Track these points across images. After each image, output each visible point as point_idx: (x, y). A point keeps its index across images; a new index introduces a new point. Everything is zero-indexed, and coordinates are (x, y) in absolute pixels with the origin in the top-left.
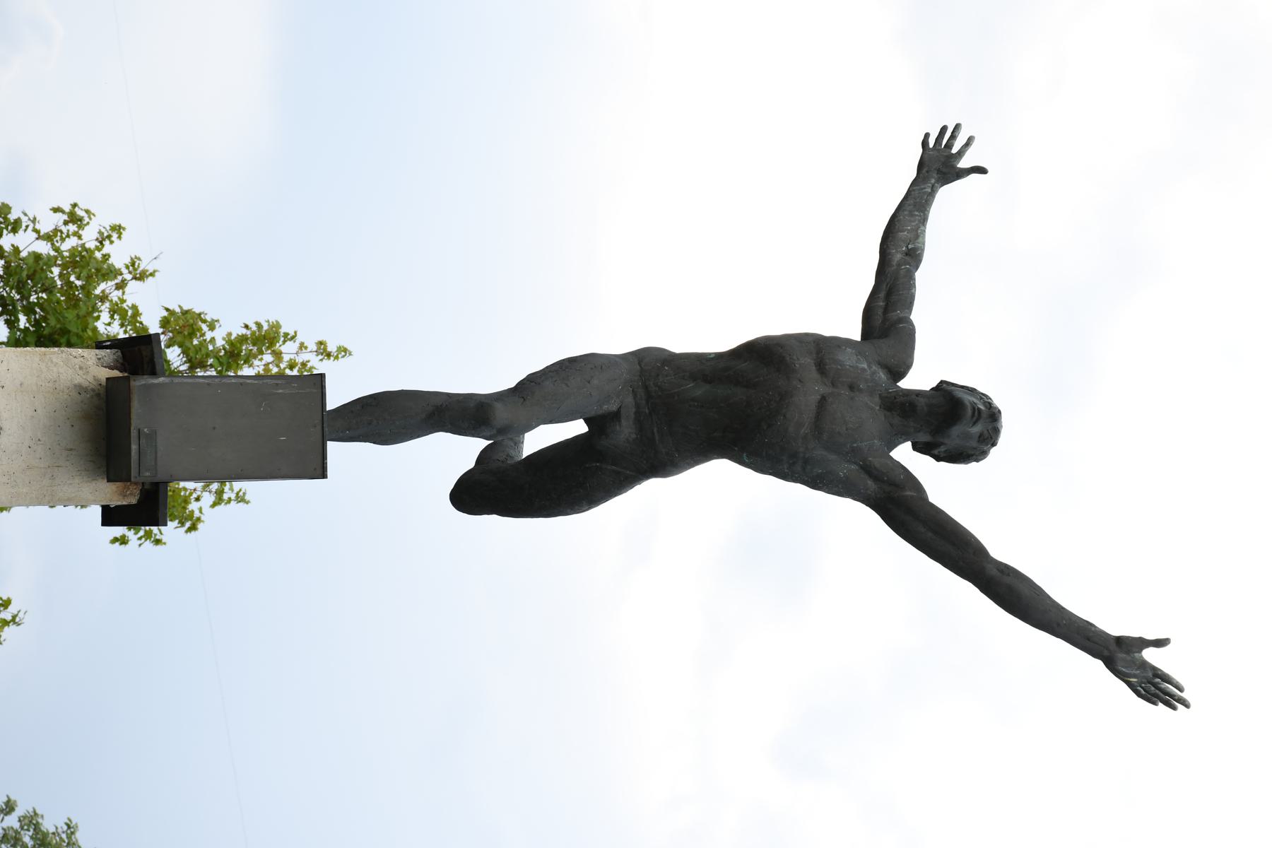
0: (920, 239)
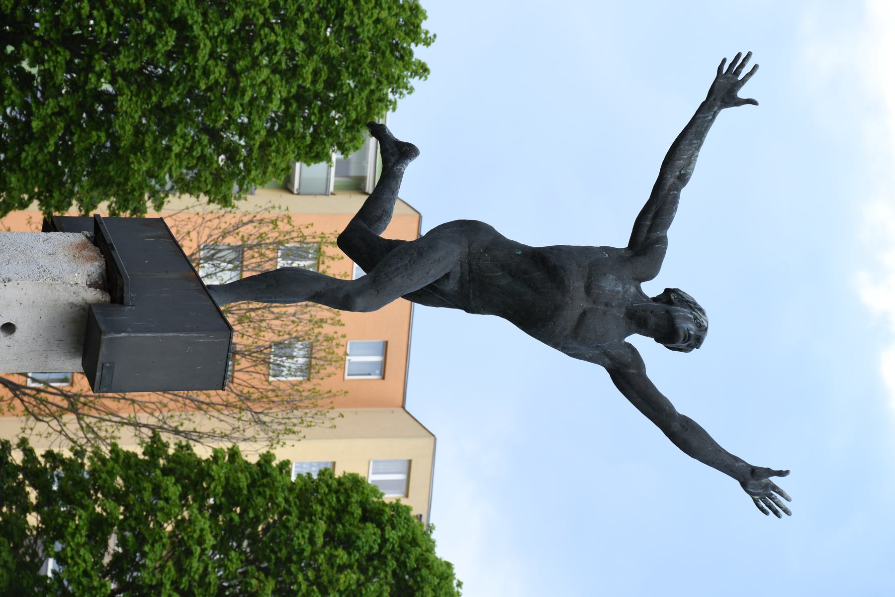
0: (692, 165)
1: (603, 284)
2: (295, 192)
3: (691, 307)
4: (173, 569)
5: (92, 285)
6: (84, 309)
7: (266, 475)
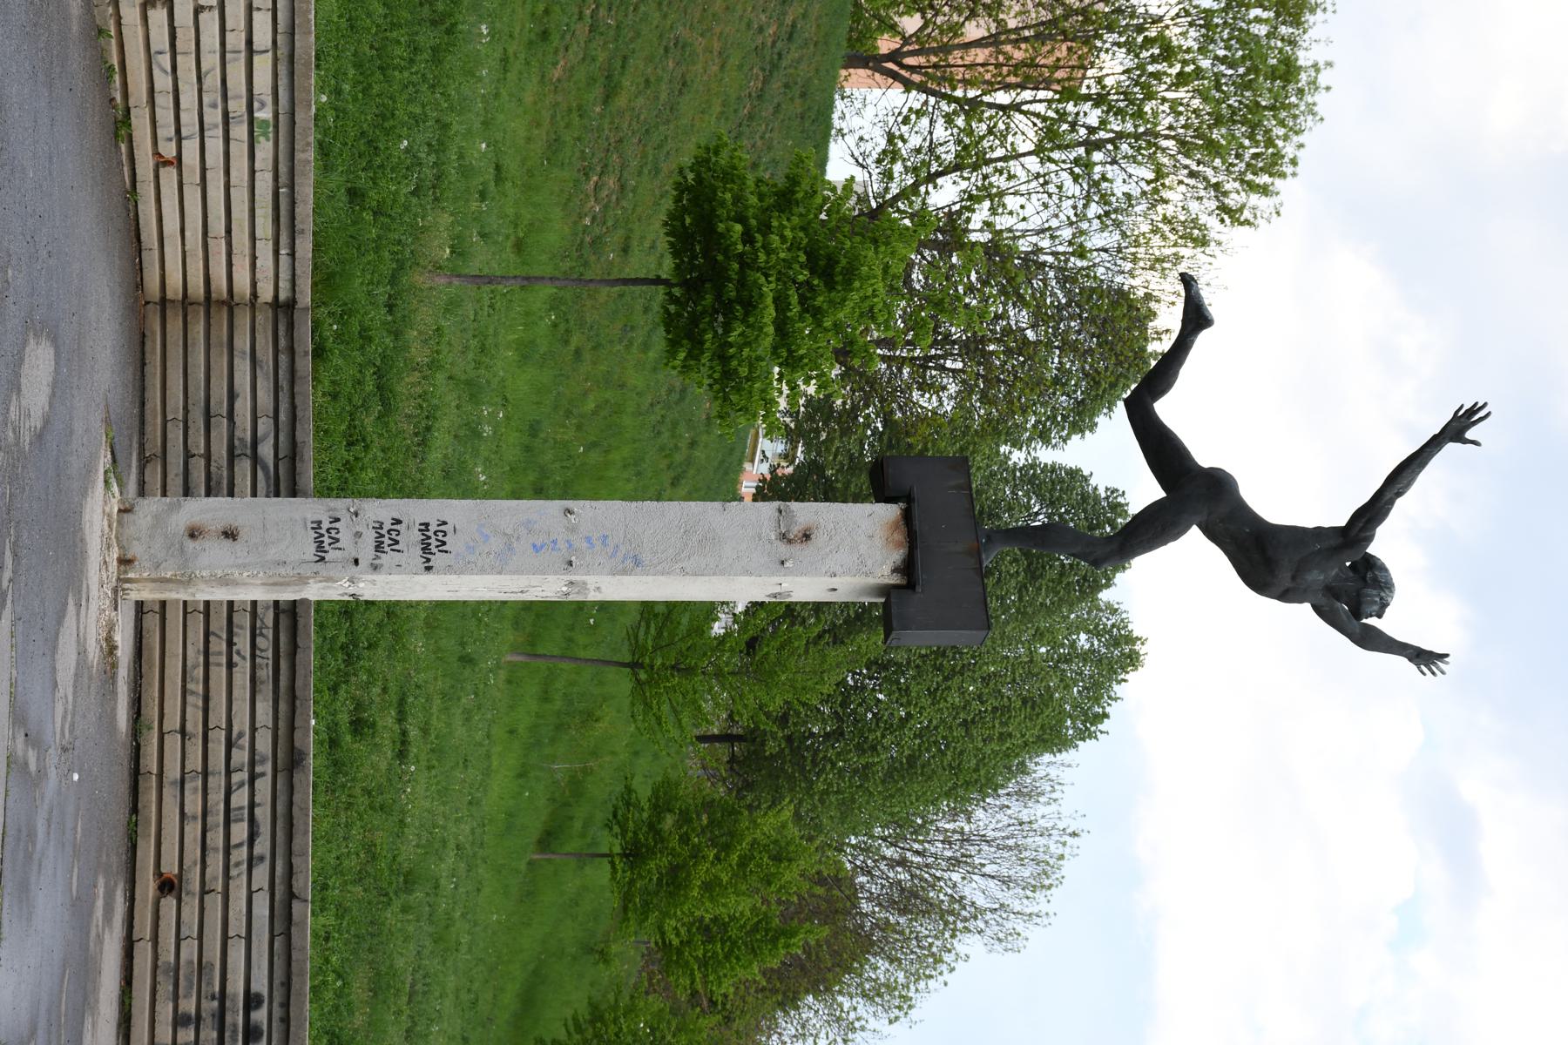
2: (311, 491)
5: (895, 570)
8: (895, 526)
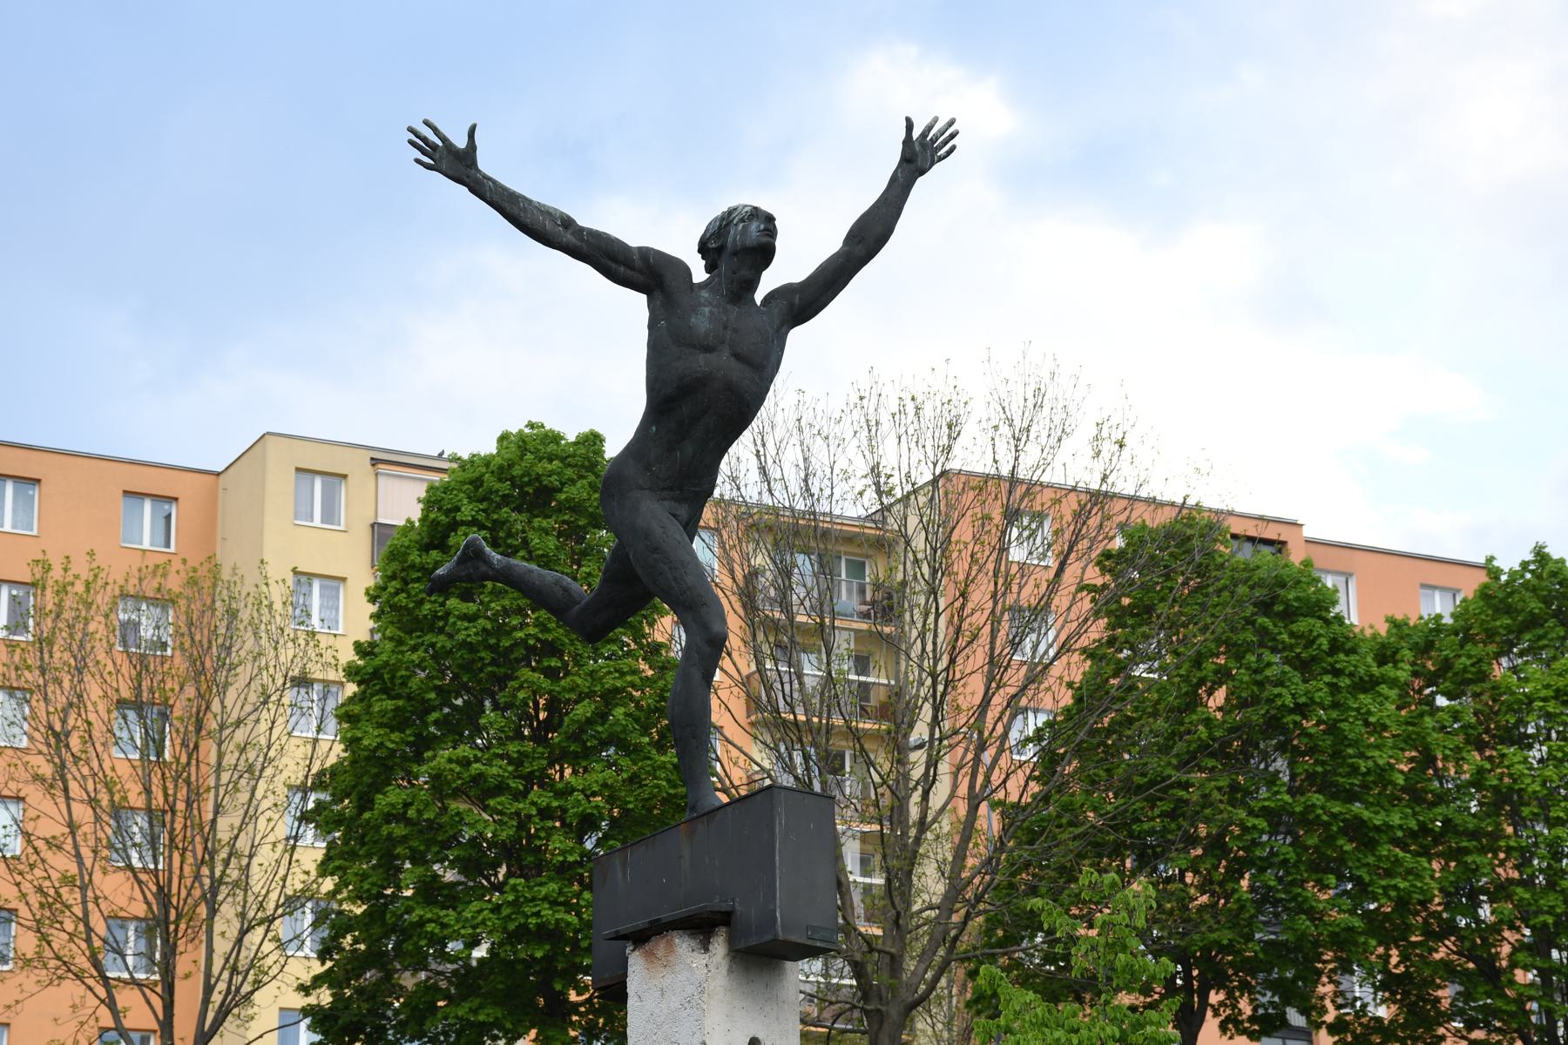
1: (703, 330)
3: (727, 225)
4: (499, 799)
6: (734, 957)
7: (376, 674)
8: (651, 956)
